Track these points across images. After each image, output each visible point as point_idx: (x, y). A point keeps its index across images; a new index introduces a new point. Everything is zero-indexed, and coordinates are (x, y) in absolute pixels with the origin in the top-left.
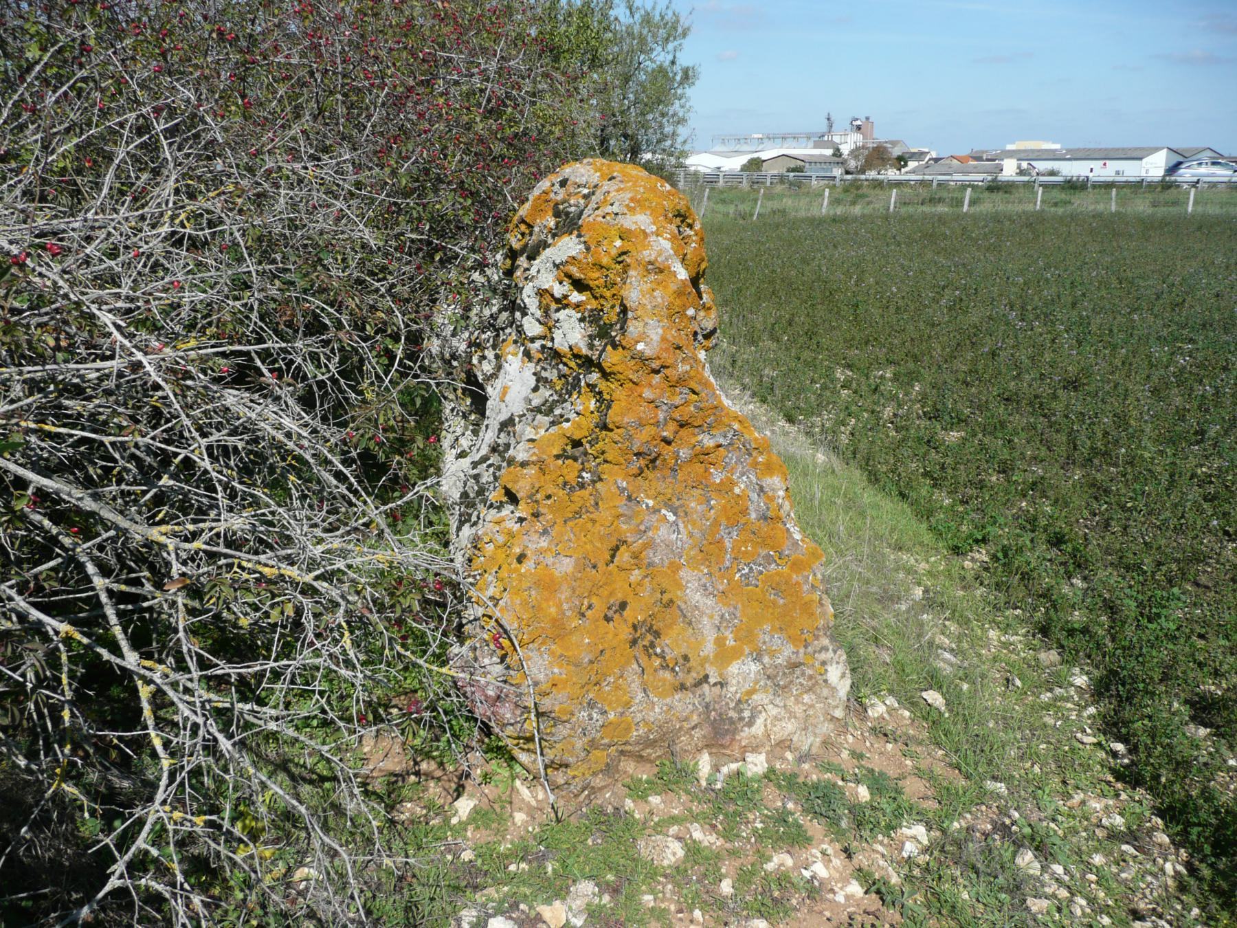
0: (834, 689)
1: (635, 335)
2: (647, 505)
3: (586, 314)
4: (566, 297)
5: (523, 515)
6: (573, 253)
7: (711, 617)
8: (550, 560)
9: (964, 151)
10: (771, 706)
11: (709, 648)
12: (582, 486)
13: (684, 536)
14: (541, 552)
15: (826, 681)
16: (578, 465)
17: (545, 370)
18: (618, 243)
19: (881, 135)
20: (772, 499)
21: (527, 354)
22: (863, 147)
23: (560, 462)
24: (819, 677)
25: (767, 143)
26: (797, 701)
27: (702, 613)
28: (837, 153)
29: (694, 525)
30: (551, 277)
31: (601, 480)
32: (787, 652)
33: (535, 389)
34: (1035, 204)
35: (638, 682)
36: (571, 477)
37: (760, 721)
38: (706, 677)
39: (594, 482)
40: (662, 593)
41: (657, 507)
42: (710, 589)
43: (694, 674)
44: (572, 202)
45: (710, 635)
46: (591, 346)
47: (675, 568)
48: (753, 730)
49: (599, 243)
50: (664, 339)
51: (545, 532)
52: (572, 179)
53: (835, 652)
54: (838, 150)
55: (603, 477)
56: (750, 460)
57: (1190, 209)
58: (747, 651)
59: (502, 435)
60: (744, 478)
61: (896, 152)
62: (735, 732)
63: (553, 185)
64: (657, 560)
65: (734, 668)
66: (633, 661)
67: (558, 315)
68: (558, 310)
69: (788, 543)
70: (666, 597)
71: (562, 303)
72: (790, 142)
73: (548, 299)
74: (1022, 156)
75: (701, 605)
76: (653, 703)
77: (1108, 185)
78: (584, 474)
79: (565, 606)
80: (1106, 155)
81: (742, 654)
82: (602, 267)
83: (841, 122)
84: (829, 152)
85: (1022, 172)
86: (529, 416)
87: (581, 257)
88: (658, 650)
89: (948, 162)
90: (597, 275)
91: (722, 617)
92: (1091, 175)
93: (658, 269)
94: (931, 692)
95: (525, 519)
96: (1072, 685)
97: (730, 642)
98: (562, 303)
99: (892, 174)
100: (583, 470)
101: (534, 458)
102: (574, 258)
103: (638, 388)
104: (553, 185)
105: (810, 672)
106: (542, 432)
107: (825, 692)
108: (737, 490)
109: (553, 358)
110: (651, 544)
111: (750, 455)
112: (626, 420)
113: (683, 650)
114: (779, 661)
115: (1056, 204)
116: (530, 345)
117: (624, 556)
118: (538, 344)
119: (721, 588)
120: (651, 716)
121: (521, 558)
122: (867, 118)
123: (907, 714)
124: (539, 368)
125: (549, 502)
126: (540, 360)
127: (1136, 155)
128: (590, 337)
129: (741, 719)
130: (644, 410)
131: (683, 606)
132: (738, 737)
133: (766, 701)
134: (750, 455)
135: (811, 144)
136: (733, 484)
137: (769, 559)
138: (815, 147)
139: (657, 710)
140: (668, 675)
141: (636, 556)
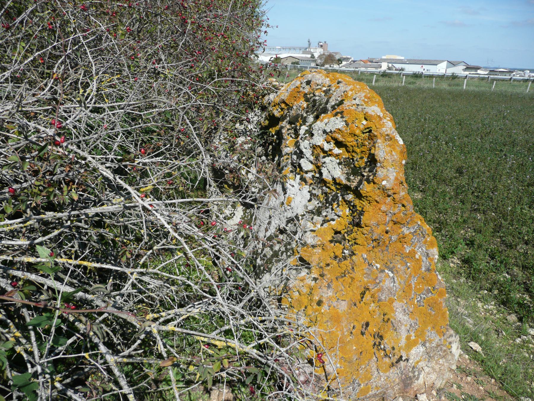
0: (453, 356)
1: (382, 177)
2: (377, 267)
3: (342, 160)
4: (330, 150)
5: (316, 276)
6: (340, 127)
7: (406, 326)
8: (335, 303)
9: (365, 58)
10: (426, 367)
11: (403, 342)
12: (345, 258)
13: (397, 284)
14: (329, 299)
15: (451, 352)
16: (341, 246)
17: (315, 189)
18: (364, 122)
19: (331, 50)
20: (432, 260)
21: (303, 179)
22: (324, 54)
23: (333, 244)
24: (449, 351)
25: (283, 51)
26: (437, 363)
27: (402, 324)
28: (313, 56)
29: (401, 278)
30: (322, 139)
31: (354, 254)
32: (436, 339)
33: (310, 200)
34: (402, 82)
35: (375, 366)
36: (339, 253)
37: (421, 376)
38: (401, 357)
39: (351, 256)
40: (384, 315)
41: (382, 268)
42: (407, 311)
43: (396, 357)
44: (317, 94)
45: (404, 334)
46: (348, 179)
47: (391, 301)
48: (419, 381)
49: (353, 122)
50: (396, 179)
51: (329, 287)
52: (313, 80)
53: (455, 337)
54: (313, 55)
55: (355, 252)
56: (424, 240)
57: (464, 87)
58: (420, 341)
59: (289, 225)
60: (420, 249)
61: (337, 57)
62: (411, 383)
63: (302, 83)
64: (383, 298)
65: (413, 351)
66: (374, 356)
67: (324, 160)
68: (324, 157)
69: (437, 282)
70: (386, 317)
71: (327, 154)
72: (292, 51)
73: (319, 150)
74: (389, 61)
75: (402, 320)
76: (381, 376)
77: (431, 77)
78: (345, 251)
79: (345, 330)
80: (423, 63)
81: (417, 343)
82: (355, 135)
83: (314, 44)
84: (309, 56)
85: (389, 68)
86: (307, 215)
87: (344, 129)
88: (382, 347)
89: (359, 62)
90: (352, 139)
91: (411, 325)
92: (424, 72)
93: (389, 138)
94: (472, 343)
95: (317, 279)
96: (530, 334)
97: (413, 338)
98: (327, 154)
99: (336, 67)
100: (344, 248)
101: (319, 243)
102: (339, 130)
103: (379, 205)
104: (302, 83)
105: (445, 348)
106: (319, 226)
107: (450, 357)
108: (417, 257)
109: (319, 183)
110: (381, 290)
111: (424, 237)
112: (372, 222)
113: (392, 345)
114: (433, 345)
115: (410, 83)
116: (305, 175)
117: (367, 297)
118: (310, 175)
119: (411, 310)
120: (380, 383)
121: (320, 303)
122: (325, 42)
123: (467, 356)
124: (311, 188)
125: (329, 268)
126: (312, 184)
127: (435, 63)
128: (347, 174)
129: (414, 376)
130: (380, 216)
131: (393, 321)
132: (413, 386)
133: (424, 365)
134: (424, 237)
135: (301, 52)
136: (415, 253)
137: (428, 291)
138: (303, 54)
139: (382, 379)
140: (387, 360)
141: (373, 296)
